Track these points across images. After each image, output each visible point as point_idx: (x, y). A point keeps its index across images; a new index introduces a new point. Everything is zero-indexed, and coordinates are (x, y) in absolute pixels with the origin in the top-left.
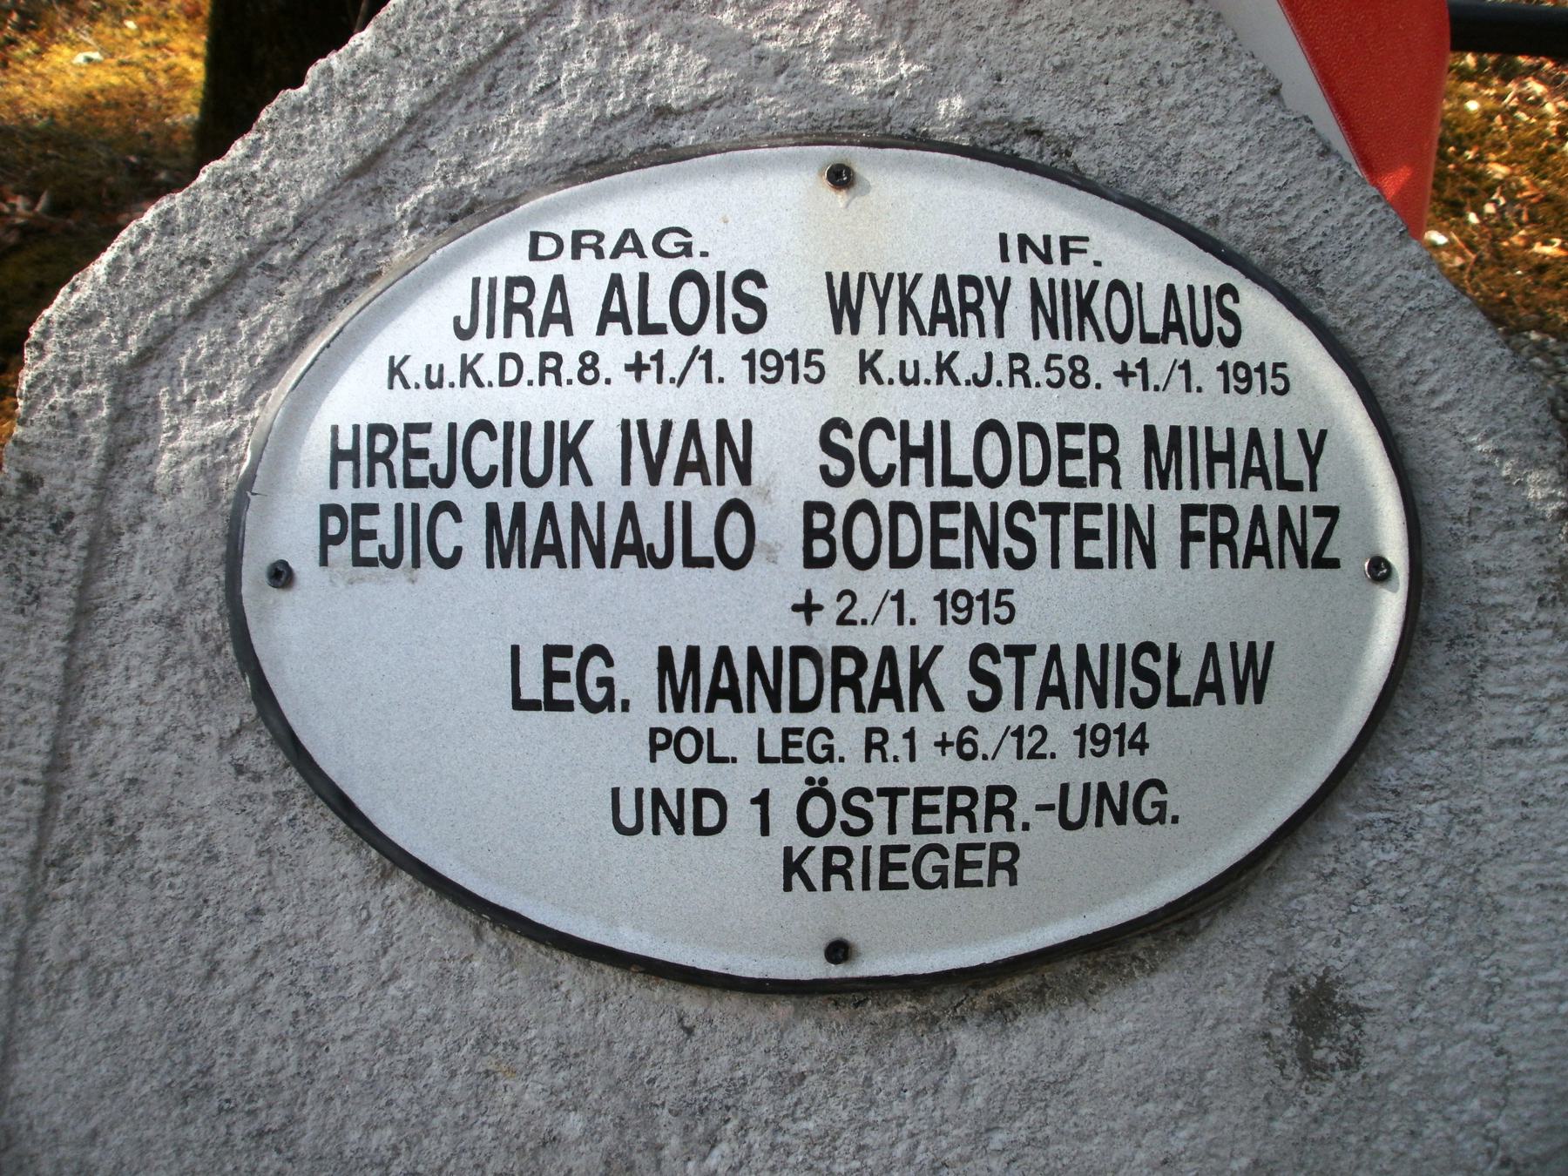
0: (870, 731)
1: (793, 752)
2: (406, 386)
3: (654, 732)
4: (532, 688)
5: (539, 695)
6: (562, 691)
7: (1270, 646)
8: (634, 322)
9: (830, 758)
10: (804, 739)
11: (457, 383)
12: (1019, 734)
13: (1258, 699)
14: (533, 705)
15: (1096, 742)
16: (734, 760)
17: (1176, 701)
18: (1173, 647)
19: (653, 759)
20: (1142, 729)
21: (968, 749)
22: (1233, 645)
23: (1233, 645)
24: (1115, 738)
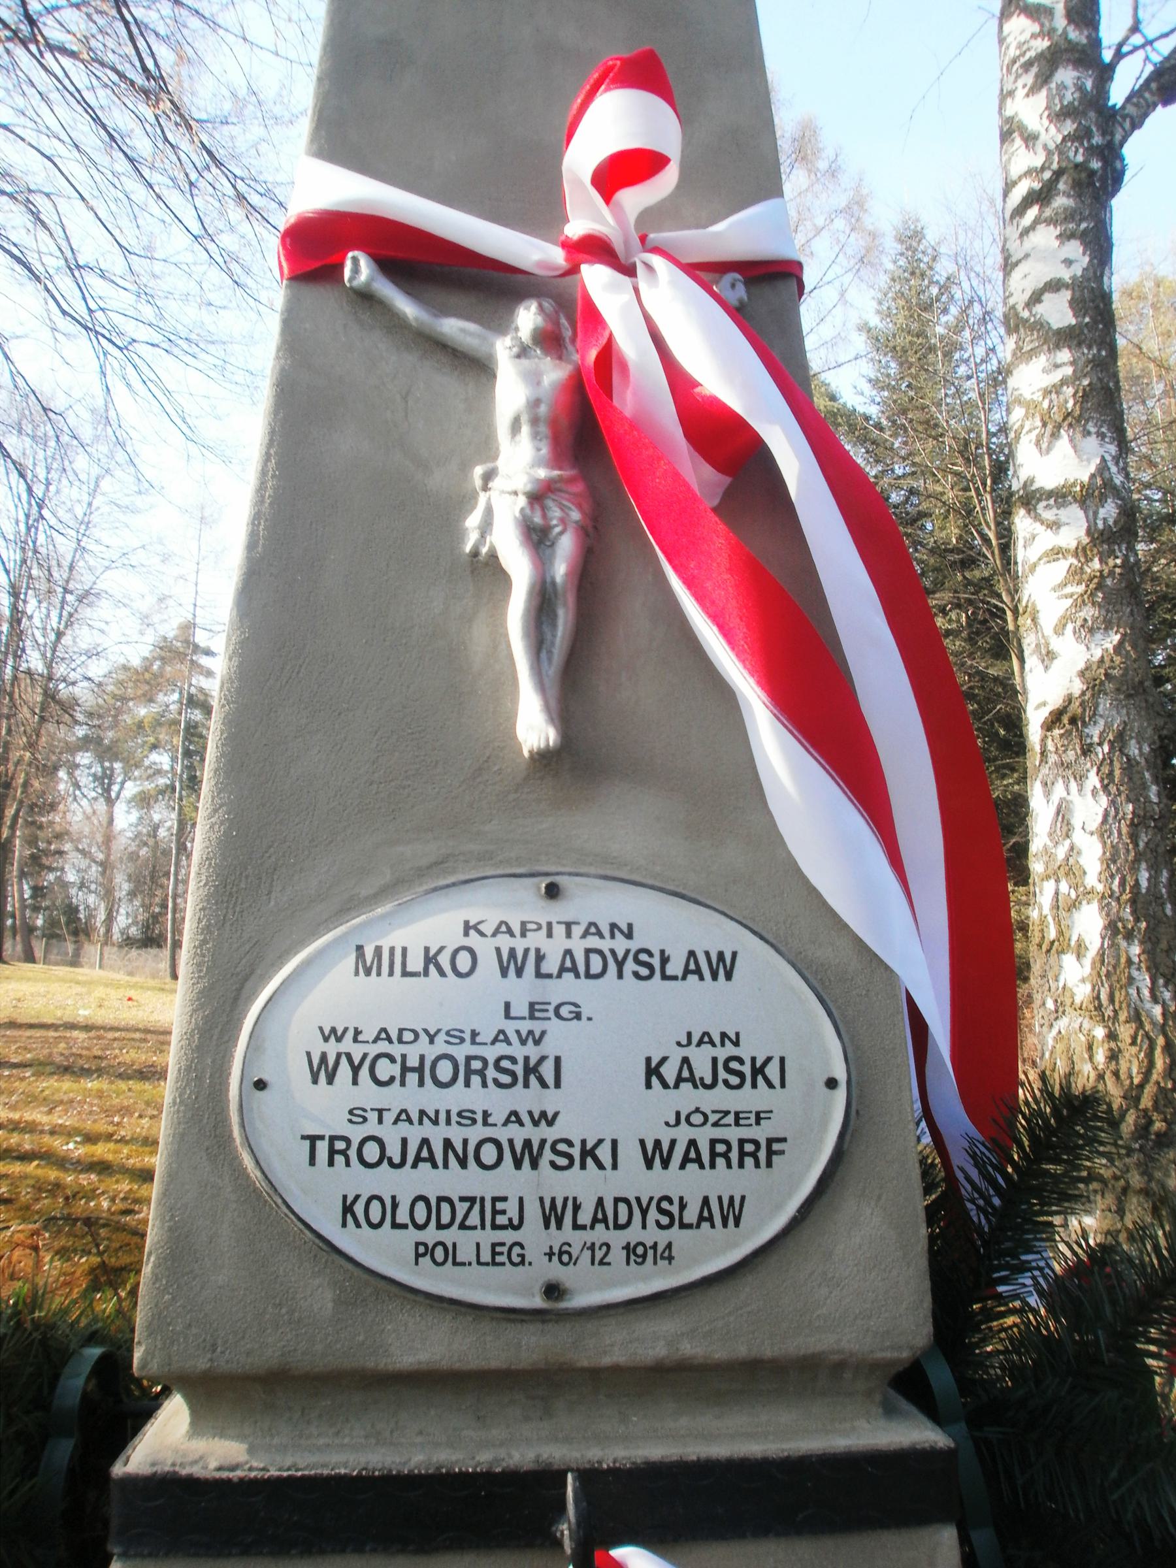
1: (498, 1259)
3: (417, 1244)
7: (743, 1198)
9: (522, 1262)
10: (505, 1249)
12: (592, 1248)
13: (737, 1224)
15: (635, 1255)
17: (683, 1226)
18: (681, 1199)
19: (417, 1263)
21: (565, 1258)
22: (720, 1198)
23: (720, 1198)
24: (650, 1253)
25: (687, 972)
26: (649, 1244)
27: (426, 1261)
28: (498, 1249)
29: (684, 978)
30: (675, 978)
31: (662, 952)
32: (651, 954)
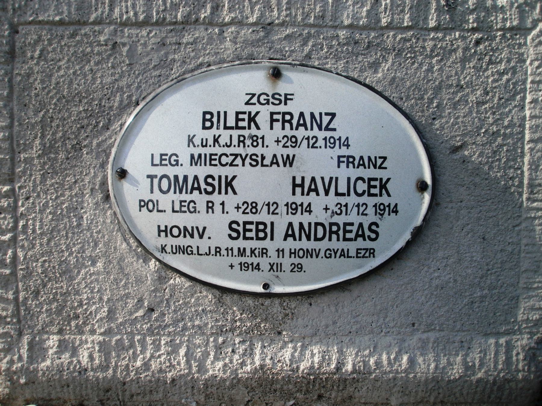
0: (208, 202)
2: (195, 146)
4: (177, 208)
5: (179, 210)
6: (184, 209)
8: (346, 255)
10: (186, 204)
11: (212, 145)
12: (268, 205)
14: (177, 212)
16: (165, 211)
19: (140, 211)
20: (309, 205)
25: (272, 163)
26: (250, 263)
27: (144, 209)
28: (183, 204)
29: (271, 166)
30: (267, 166)
31: (262, 155)
32: (257, 156)
